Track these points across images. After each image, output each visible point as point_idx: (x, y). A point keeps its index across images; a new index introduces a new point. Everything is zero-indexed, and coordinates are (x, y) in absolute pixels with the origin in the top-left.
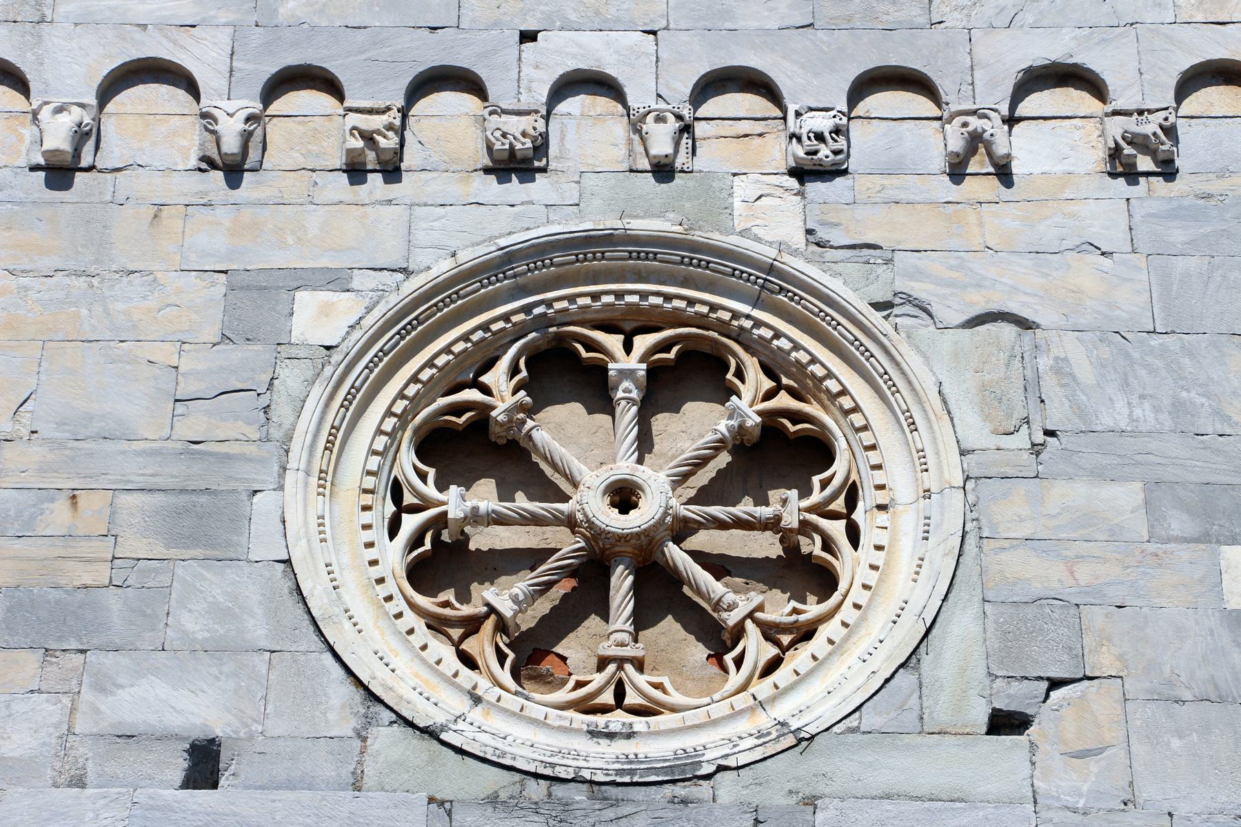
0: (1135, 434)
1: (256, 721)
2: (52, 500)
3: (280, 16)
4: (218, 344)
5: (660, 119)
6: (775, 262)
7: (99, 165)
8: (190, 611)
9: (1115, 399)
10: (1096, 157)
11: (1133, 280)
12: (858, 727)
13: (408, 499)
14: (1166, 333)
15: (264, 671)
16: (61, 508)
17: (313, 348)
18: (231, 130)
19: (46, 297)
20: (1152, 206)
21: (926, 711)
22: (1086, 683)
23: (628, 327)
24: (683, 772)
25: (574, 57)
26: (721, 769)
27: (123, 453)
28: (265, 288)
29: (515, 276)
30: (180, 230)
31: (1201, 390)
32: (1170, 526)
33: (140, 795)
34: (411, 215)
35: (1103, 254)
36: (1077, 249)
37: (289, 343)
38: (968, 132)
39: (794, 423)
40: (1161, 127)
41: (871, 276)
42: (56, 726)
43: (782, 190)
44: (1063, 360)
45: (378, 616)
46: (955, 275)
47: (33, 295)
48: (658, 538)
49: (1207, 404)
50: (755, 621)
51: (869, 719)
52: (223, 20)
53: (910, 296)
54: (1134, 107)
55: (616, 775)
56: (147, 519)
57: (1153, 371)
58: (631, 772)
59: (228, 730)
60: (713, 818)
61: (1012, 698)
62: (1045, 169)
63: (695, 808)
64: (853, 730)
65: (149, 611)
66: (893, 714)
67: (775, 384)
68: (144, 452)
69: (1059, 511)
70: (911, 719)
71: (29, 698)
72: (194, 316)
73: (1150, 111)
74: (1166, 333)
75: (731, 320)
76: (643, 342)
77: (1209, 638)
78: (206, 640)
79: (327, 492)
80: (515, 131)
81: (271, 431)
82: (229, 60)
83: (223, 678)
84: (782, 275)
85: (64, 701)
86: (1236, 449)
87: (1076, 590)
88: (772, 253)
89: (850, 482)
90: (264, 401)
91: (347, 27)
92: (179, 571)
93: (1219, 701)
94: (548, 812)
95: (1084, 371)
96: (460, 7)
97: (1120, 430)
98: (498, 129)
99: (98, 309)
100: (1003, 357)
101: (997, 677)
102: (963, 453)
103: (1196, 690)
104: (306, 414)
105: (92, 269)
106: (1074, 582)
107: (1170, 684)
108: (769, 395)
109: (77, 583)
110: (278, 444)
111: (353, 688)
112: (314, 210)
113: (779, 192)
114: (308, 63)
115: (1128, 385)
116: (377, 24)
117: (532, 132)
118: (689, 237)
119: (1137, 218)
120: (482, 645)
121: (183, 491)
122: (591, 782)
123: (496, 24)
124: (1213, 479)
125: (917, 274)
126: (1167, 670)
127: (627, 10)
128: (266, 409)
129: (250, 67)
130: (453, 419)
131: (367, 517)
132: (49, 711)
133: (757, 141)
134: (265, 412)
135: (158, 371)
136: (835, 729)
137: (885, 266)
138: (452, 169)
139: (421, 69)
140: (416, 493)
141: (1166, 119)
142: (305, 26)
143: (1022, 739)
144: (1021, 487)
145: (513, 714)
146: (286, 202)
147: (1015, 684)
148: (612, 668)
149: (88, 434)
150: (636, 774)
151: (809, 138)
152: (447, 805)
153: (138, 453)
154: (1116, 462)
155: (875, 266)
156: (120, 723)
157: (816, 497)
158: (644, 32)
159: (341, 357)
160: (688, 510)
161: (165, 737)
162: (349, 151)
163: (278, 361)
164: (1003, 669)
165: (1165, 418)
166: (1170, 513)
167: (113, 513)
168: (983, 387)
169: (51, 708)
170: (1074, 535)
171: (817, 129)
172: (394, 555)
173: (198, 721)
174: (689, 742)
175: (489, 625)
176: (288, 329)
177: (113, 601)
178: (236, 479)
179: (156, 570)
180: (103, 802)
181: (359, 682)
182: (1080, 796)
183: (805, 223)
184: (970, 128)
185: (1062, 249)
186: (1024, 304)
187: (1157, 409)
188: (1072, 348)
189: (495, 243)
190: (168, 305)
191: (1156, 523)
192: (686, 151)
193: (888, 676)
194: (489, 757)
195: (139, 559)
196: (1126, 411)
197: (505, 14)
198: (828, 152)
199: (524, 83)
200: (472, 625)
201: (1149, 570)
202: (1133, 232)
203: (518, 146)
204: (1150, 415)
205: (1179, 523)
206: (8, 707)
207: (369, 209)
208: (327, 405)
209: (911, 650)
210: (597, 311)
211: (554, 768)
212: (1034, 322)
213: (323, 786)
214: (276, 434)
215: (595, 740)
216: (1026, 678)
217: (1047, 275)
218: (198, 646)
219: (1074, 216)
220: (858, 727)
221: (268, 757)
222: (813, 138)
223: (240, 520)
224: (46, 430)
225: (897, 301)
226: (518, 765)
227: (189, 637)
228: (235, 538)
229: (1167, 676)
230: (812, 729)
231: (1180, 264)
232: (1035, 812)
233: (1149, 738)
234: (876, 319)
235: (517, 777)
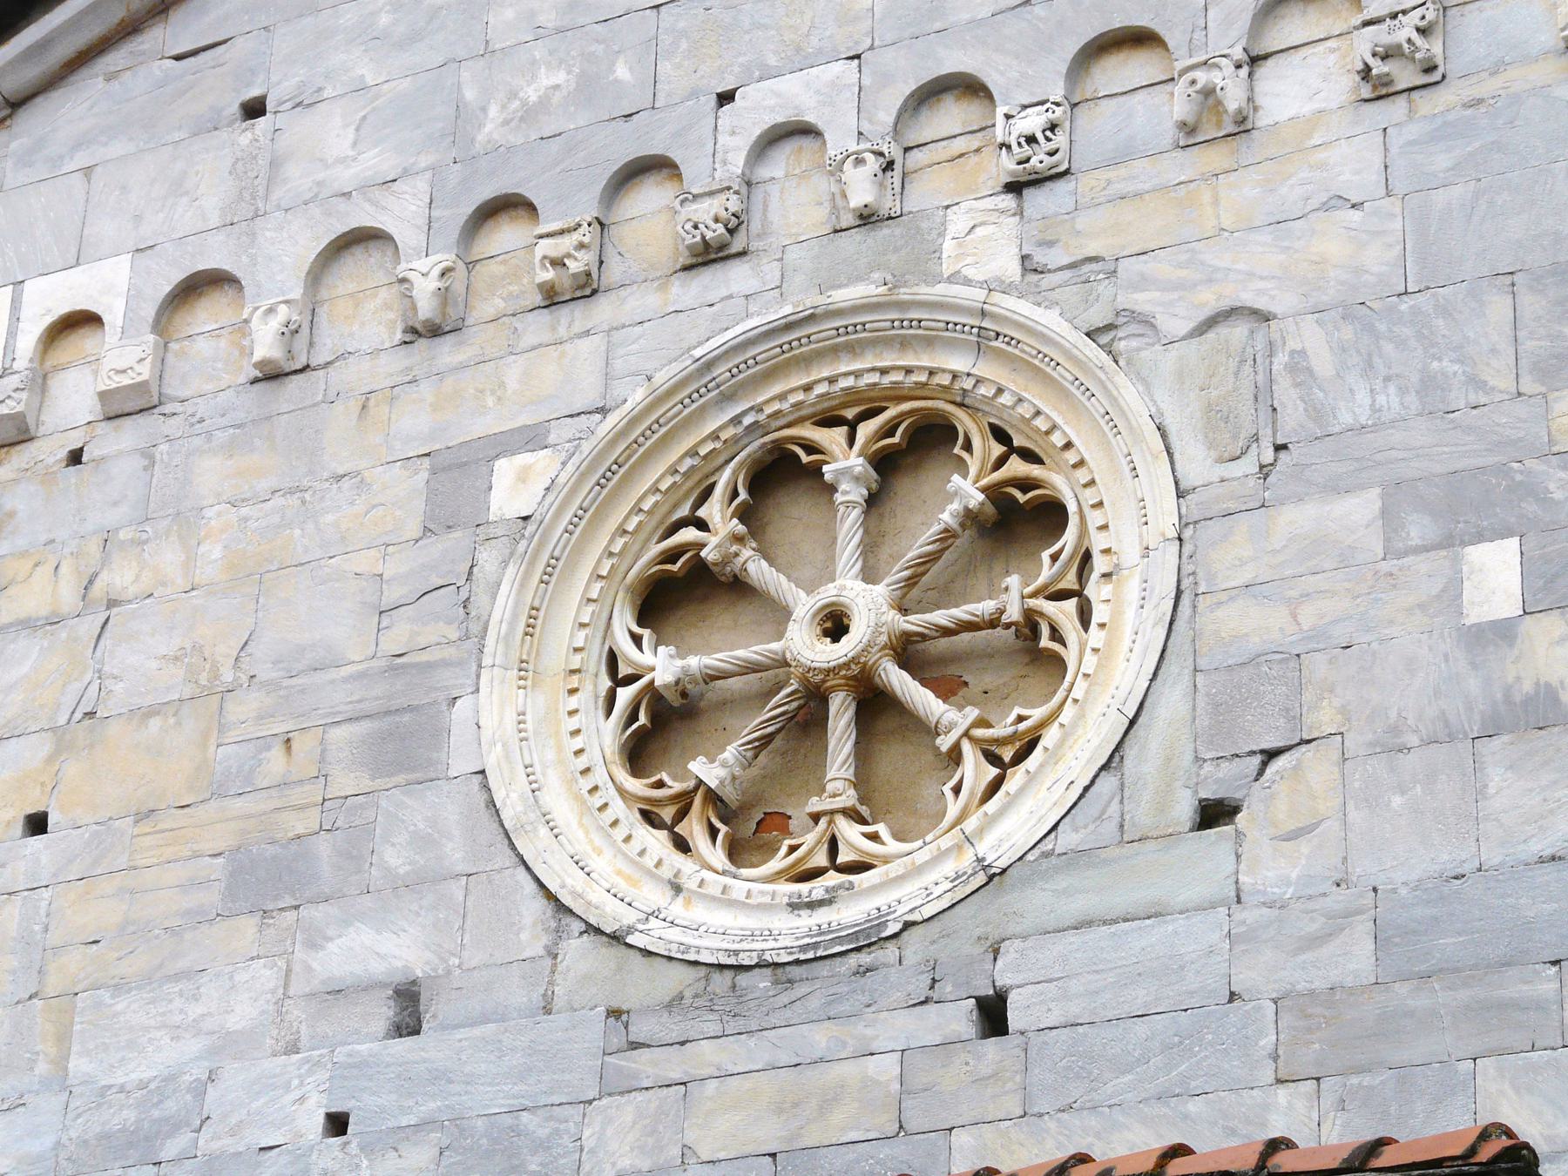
0: (1377, 427)
1: (454, 955)
2: (269, 748)
3: (477, 145)
4: (421, 538)
5: (859, 162)
6: (985, 306)
7: (313, 365)
8: (393, 845)
9: (1355, 388)
10: (1344, 85)
11: (1384, 231)
12: (1053, 850)
13: (623, 670)
14: (1419, 291)
15: (461, 898)
16: (277, 753)
17: (511, 522)
18: (425, 289)
19: (264, 524)
20: (1413, 131)
21: (1127, 817)
22: (1304, 748)
23: (850, 414)
24: (868, 936)
25: (772, 109)
26: (908, 925)
27: (332, 682)
28: (465, 464)
29: (718, 386)
30: (386, 418)
31: (1453, 355)
32: (1409, 535)
33: (341, 1054)
34: (608, 342)
35: (1353, 206)
36: (1325, 207)
37: (487, 522)
38: (1196, 92)
39: (1025, 490)
40: (1418, 30)
41: (1091, 298)
42: (273, 992)
43: (997, 214)
44: (1299, 352)
45: (582, 814)
46: (1183, 273)
47: (252, 525)
48: (870, 663)
49: (1460, 371)
50: (971, 739)
51: (1067, 839)
52: (423, 165)
53: (1134, 312)
54: (1385, 12)
55: (800, 952)
56: (354, 751)
57: (1401, 344)
58: (815, 946)
59: (427, 969)
60: (889, 985)
61: (1217, 783)
62: (1291, 113)
63: (872, 976)
64: (1046, 855)
65: (355, 853)
66: (1092, 827)
67: (1006, 448)
68: (351, 676)
69: (1284, 543)
70: (1110, 828)
71: (249, 966)
72: (398, 513)
73: (1404, 12)
74: (1419, 291)
75: (952, 383)
76: (865, 430)
77: (1443, 665)
78: (407, 873)
79: (529, 683)
80: (706, 217)
81: (470, 626)
82: (427, 211)
83: (423, 913)
84: (995, 317)
85: (280, 964)
86: (1490, 422)
87: (1300, 637)
88: (979, 294)
89: (1083, 550)
90: (464, 594)
91: (542, 138)
92: (383, 803)
93: (1448, 740)
94: (722, 1008)
95: (1323, 362)
96: (655, 82)
97: (1359, 427)
98: (689, 220)
99: (310, 526)
100: (1233, 364)
101: (1205, 761)
102: (1180, 495)
103: (1424, 731)
104: (501, 600)
105: (305, 483)
106: (1296, 627)
107: (1395, 730)
108: (1001, 462)
109: (291, 835)
110: (476, 640)
111: (545, 901)
112: (515, 362)
113: (993, 217)
114: (504, 192)
115: (1371, 366)
116: (572, 127)
117: (723, 214)
118: (894, 297)
119: (1394, 150)
120: (693, 827)
121: (388, 713)
122: (776, 965)
123: (694, 94)
124: (1459, 466)
125: (1143, 283)
126: (1393, 715)
127: (829, 37)
128: (466, 604)
129: (447, 213)
130: (668, 567)
131: (573, 702)
132: (266, 976)
133: (974, 159)
134: (465, 607)
135: (365, 583)
136: (1030, 857)
137: (1107, 281)
138: (651, 278)
139: (616, 168)
140: (630, 662)
141: (1423, 17)
142: (502, 149)
143: (1227, 829)
144: (1243, 523)
145: (714, 899)
146: (486, 358)
147: (1225, 765)
148: (823, 822)
149: (301, 668)
150: (820, 948)
151: (1019, 144)
152: (624, 1017)
153: (346, 680)
154: (1352, 467)
155: (1095, 283)
156: (329, 978)
157: (1046, 573)
158: (848, 58)
159: (535, 527)
160: (908, 622)
161: (368, 987)
162: (541, 286)
163: (477, 546)
164: (1210, 750)
165: (1412, 400)
166: (1410, 518)
167: (323, 751)
168: (1208, 407)
169: (269, 973)
170: (1301, 570)
171: (1028, 132)
172: (607, 735)
173: (399, 964)
174: (881, 901)
175: (698, 801)
176: (486, 506)
177: (323, 847)
178: (436, 689)
179: (362, 807)
180: (306, 1067)
181: (550, 896)
182: (1289, 884)
183: (1021, 250)
184: (1198, 86)
185: (1306, 211)
186: (1260, 292)
187: (1403, 391)
188: (1311, 339)
189: (691, 356)
190: (374, 506)
191: (1393, 535)
192: (892, 192)
193: (1087, 782)
194: (673, 954)
195: (346, 797)
196: (1368, 401)
197: (703, 77)
198: (1042, 156)
199: (719, 157)
200: (683, 803)
201: (1380, 595)
202: (1389, 170)
203: (709, 235)
204: (1395, 401)
205: (1418, 529)
206: (231, 978)
207: (567, 346)
208: (522, 585)
209: (1113, 747)
210: (813, 405)
211: (737, 955)
212: (1269, 313)
213: (515, 1015)
214: (475, 628)
215: (796, 912)
216: (1237, 756)
217: (1288, 248)
218: (400, 882)
219: (1322, 166)
220: (1053, 850)
221: (464, 991)
222: (1024, 143)
223: (439, 734)
224: (266, 673)
225: (1121, 320)
226: (702, 959)
227: (391, 873)
228: (435, 755)
229: (1392, 721)
230: (1002, 863)
231: (1440, 197)
232: (1229, 916)
233: (1367, 800)
234: (1091, 350)
235: (703, 971)
